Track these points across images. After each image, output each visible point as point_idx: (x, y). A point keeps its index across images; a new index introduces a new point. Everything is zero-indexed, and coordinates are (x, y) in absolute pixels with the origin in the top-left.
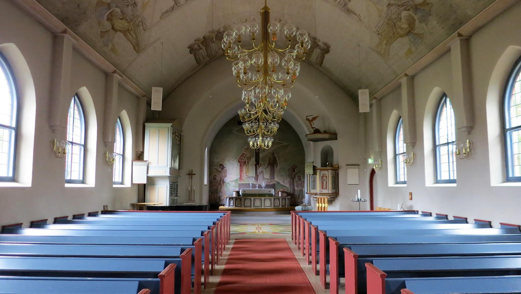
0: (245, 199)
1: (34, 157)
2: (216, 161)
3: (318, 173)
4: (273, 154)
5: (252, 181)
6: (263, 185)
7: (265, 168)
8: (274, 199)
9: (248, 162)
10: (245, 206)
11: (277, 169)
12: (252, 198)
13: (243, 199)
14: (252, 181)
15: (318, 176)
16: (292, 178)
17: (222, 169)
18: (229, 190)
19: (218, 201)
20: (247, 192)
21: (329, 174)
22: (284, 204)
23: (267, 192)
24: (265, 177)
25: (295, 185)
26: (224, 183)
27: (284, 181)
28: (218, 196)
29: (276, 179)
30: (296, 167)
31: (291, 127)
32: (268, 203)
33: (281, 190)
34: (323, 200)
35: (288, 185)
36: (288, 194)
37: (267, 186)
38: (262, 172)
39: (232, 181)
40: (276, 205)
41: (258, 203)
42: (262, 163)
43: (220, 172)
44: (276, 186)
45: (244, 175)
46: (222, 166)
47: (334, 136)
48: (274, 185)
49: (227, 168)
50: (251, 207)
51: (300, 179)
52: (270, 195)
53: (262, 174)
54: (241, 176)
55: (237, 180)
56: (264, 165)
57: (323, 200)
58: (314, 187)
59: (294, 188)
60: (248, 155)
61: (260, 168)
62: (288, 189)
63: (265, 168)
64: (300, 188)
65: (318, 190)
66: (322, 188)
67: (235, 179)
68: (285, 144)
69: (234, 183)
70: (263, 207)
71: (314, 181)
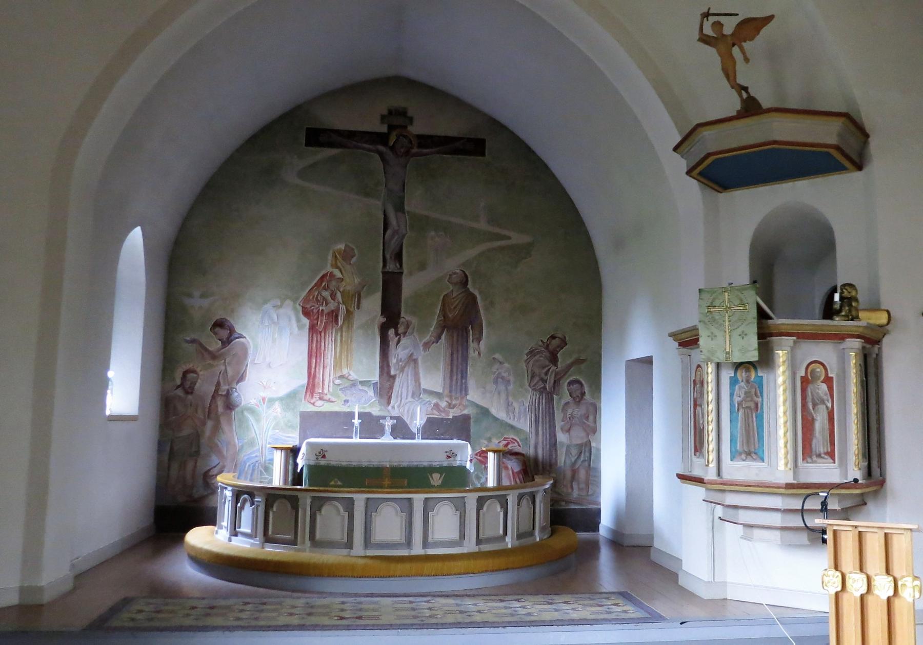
0: (318, 504)
1: (141, 378)
2: (197, 304)
3: (781, 355)
4: (465, 283)
5: (364, 402)
6: (417, 422)
7: (427, 345)
8: (481, 502)
9: (349, 315)
10: (316, 543)
11: (479, 350)
12: (360, 499)
13: (306, 502)
14: (364, 402)
15: (779, 383)
16: (547, 393)
17: (226, 342)
18: (252, 443)
19: (199, 491)
20: (333, 459)
21: (841, 360)
22: (526, 527)
23: (439, 460)
24: (424, 385)
25: (558, 424)
26: (230, 406)
27: (508, 405)
28: (202, 469)
29: (474, 395)
30: (564, 343)
31: (546, 167)
32: (445, 525)
33: (496, 443)
34: (874, 545)
35: (525, 424)
36: (531, 469)
37: (433, 428)
38: (412, 360)
39: (272, 401)
40: (486, 533)
41: (388, 525)
42: (414, 321)
43: (214, 356)
44: (473, 428)
45: (328, 376)
46: (224, 330)
47: (846, 150)
48: (466, 419)
49: (239, 330)
50: (349, 545)
51: (579, 398)
52: (455, 477)
53: (409, 371)
54: (312, 376)
55: (292, 396)
56: (423, 329)
57: (874, 545)
58: (751, 446)
59: (553, 435)
60: (351, 282)
61: (404, 341)
62: (526, 440)
63: (427, 345)
64: (578, 436)
65: (779, 463)
66: (808, 451)
67: (283, 392)
68: (517, 238)
69: (277, 406)
70: (417, 549)
71: (752, 410)
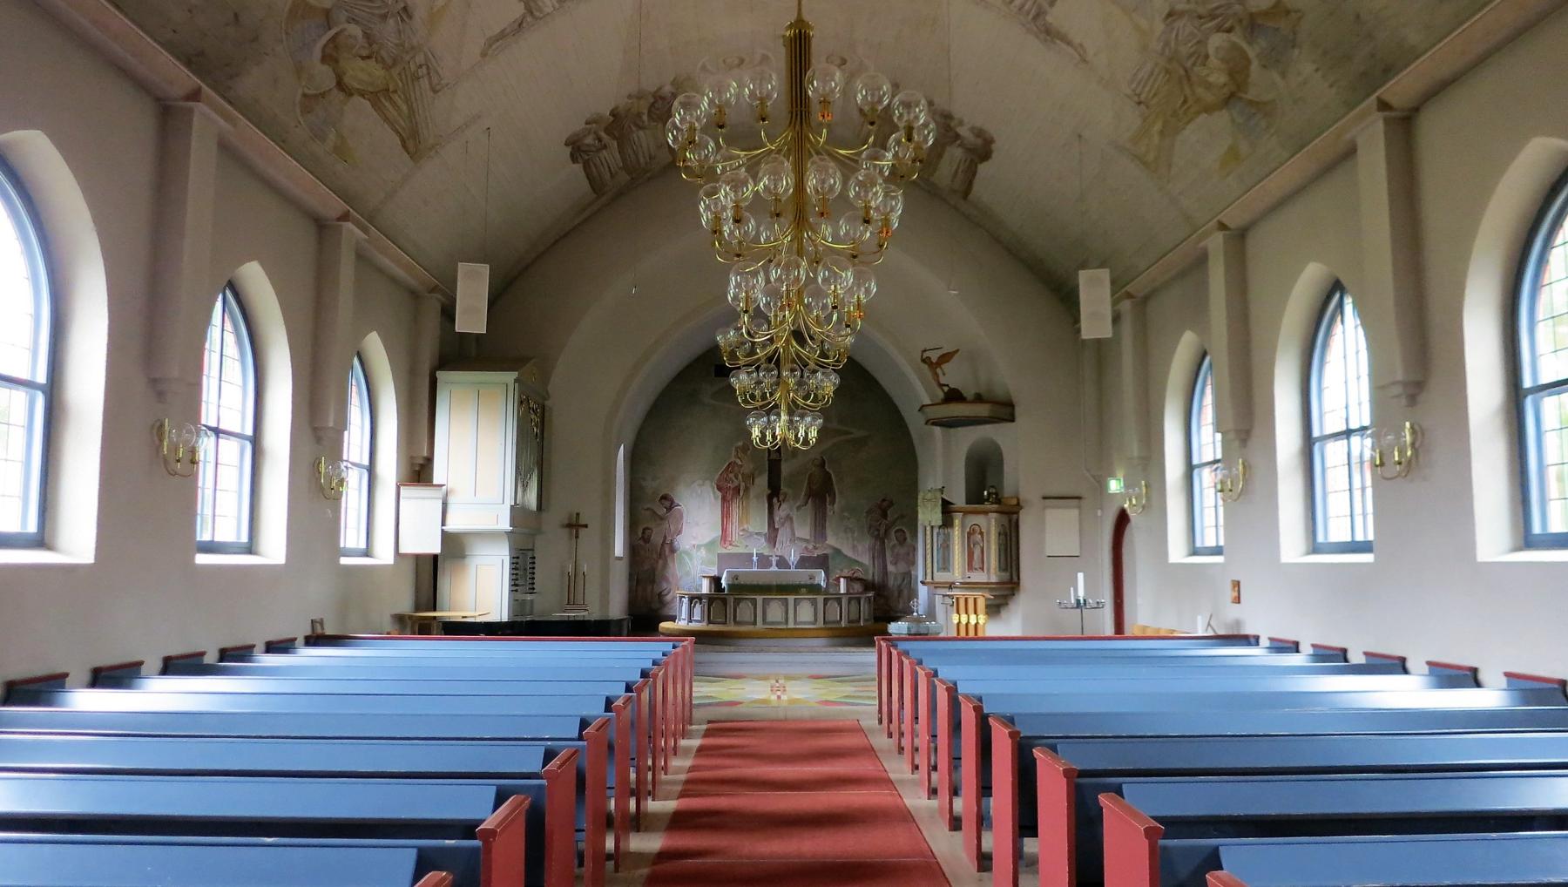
0: (737, 602)
1: (102, 473)
2: (650, 485)
3: (957, 522)
4: (823, 464)
5: (758, 547)
6: (793, 558)
7: (799, 508)
8: (826, 601)
9: (747, 489)
10: (736, 622)
11: (834, 509)
12: (760, 598)
13: (731, 600)
14: (758, 547)
15: (956, 532)
16: (880, 538)
17: (669, 509)
18: (688, 574)
19: (655, 606)
20: (742, 581)
21: (989, 524)
22: (854, 616)
23: (805, 580)
24: (797, 534)
25: (889, 558)
26: (673, 551)
27: (854, 547)
28: (657, 590)
29: (831, 540)
30: (891, 504)
31: (877, 382)
32: (805, 613)
33: (846, 573)
34: (971, 602)
35: (866, 560)
36: (868, 586)
37: (804, 562)
38: (789, 518)
39: (699, 547)
40: (830, 618)
41: (775, 612)
42: (790, 492)
43: (662, 519)
44: (831, 563)
45: (734, 528)
46: (668, 502)
47: (1004, 411)
48: (825, 557)
49: (683, 508)
50: (755, 623)
51: (902, 541)
52: (814, 589)
53: (787, 525)
54: (724, 530)
55: (712, 543)
56: (795, 498)
57: (971, 602)
58: (946, 565)
59: (885, 567)
60: (748, 467)
61: (784, 506)
62: (866, 571)
63: (799, 508)
64: (902, 567)
65: (957, 573)
66: (970, 567)
67: (708, 540)
68: (858, 433)
69: (703, 552)
70: (791, 626)
71: (946, 547)
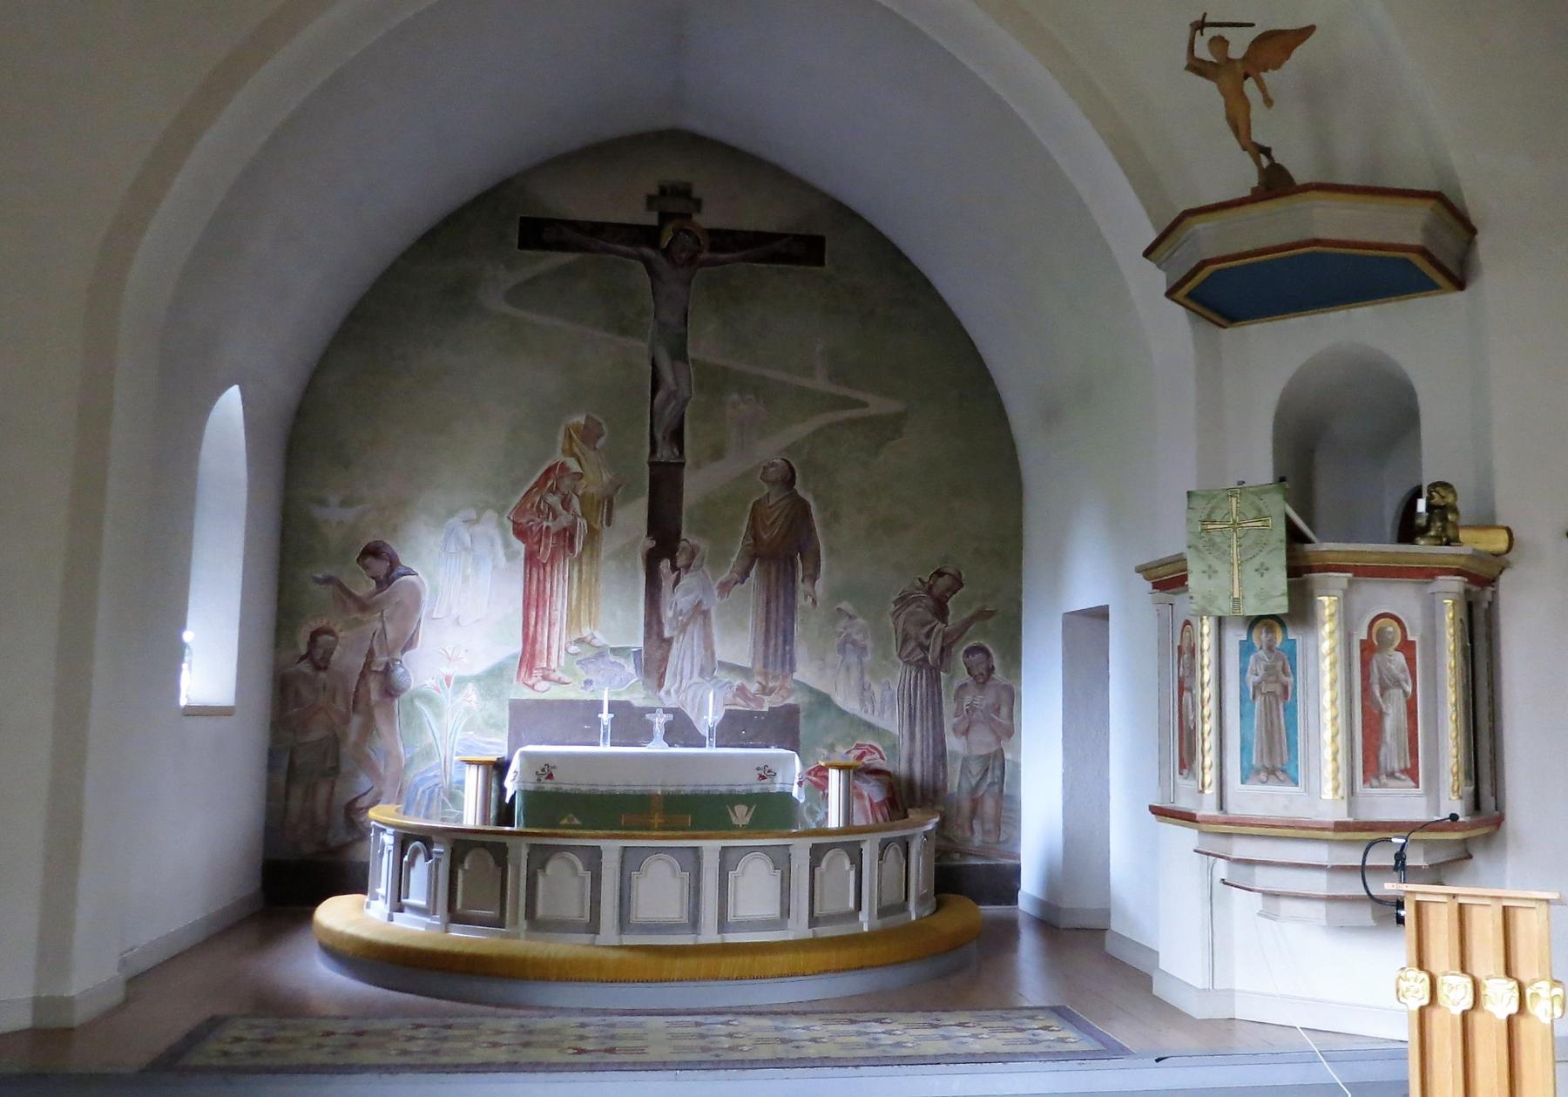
0: (540, 857)
1: (240, 642)
2: (335, 517)
3: (1327, 604)
4: (789, 481)
5: (618, 684)
6: (709, 717)
7: (725, 588)
8: (817, 853)
9: (593, 535)
10: (536, 924)
11: (813, 594)
12: (611, 848)
13: (520, 854)
14: (618, 684)
15: (1324, 651)
16: (930, 668)
17: (385, 582)
18: (428, 754)
19: (338, 836)
20: (566, 781)
21: (1429, 612)
22: (893, 896)
23: (747, 782)
24: (721, 655)
25: (949, 722)
26: (391, 691)
27: (864, 689)
28: (343, 797)
29: (805, 672)
30: (958, 583)
31: (927, 283)
32: (756, 894)
33: (843, 754)
34: (1485, 927)
35: (891, 721)
36: (902, 797)
37: (736, 728)
38: (699, 612)
39: (461, 682)
40: (826, 906)
41: (659, 892)
42: (704, 546)
43: (364, 606)
44: (804, 729)
45: (557, 639)
46: (380, 561)
47: (1437, 255)
48: (792, 712)
49: (405, 560)
50: (593, 927)
51: (983, 678)
52: (772, 812)
53: (695, 630)
54: (529, 640)
55: (496, 674)
56: (718, 559)
57: (1485, 927)
58: (1276, 758)
59: (940, 741)
60: (597, 479)
61: (686, 580)
62: (893, 748)
63: (725, 588)
64: (982, 741)
65: (1323, 788)
66: (1373, 768)
67: (480, 667)
68: (878, 405)
69: (471, 691)
70: (709, 935)
71: (1277, 697)
